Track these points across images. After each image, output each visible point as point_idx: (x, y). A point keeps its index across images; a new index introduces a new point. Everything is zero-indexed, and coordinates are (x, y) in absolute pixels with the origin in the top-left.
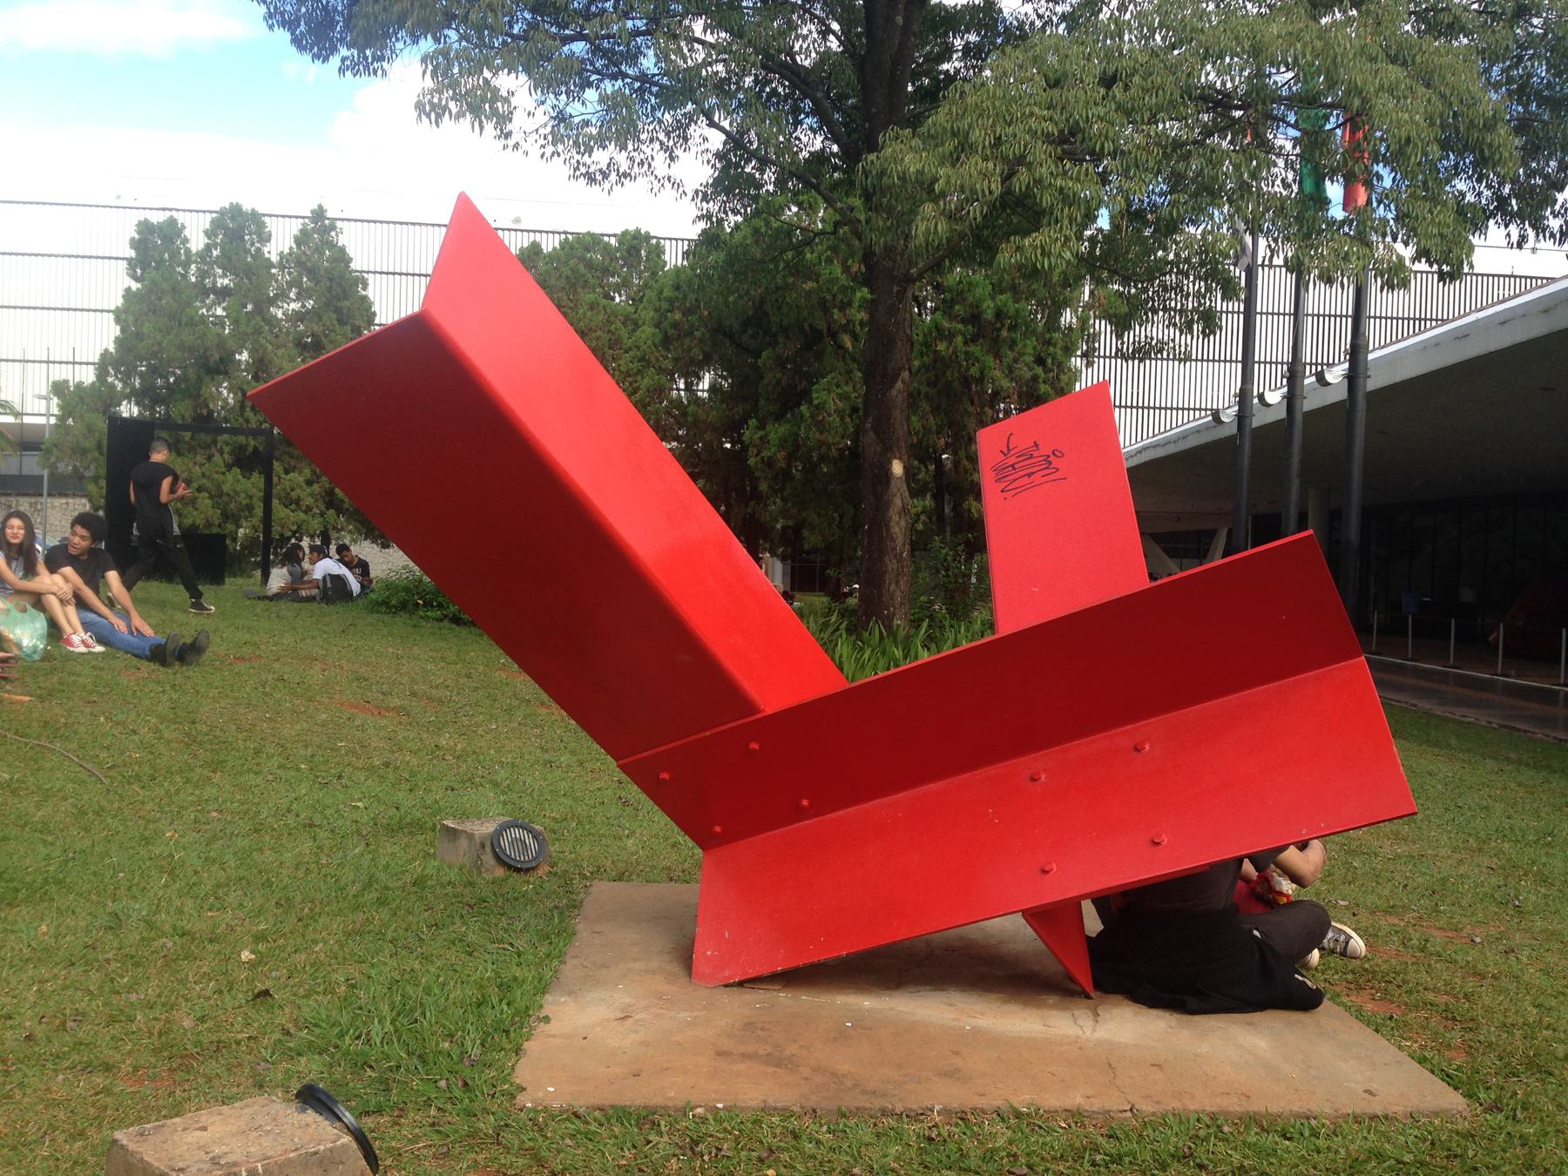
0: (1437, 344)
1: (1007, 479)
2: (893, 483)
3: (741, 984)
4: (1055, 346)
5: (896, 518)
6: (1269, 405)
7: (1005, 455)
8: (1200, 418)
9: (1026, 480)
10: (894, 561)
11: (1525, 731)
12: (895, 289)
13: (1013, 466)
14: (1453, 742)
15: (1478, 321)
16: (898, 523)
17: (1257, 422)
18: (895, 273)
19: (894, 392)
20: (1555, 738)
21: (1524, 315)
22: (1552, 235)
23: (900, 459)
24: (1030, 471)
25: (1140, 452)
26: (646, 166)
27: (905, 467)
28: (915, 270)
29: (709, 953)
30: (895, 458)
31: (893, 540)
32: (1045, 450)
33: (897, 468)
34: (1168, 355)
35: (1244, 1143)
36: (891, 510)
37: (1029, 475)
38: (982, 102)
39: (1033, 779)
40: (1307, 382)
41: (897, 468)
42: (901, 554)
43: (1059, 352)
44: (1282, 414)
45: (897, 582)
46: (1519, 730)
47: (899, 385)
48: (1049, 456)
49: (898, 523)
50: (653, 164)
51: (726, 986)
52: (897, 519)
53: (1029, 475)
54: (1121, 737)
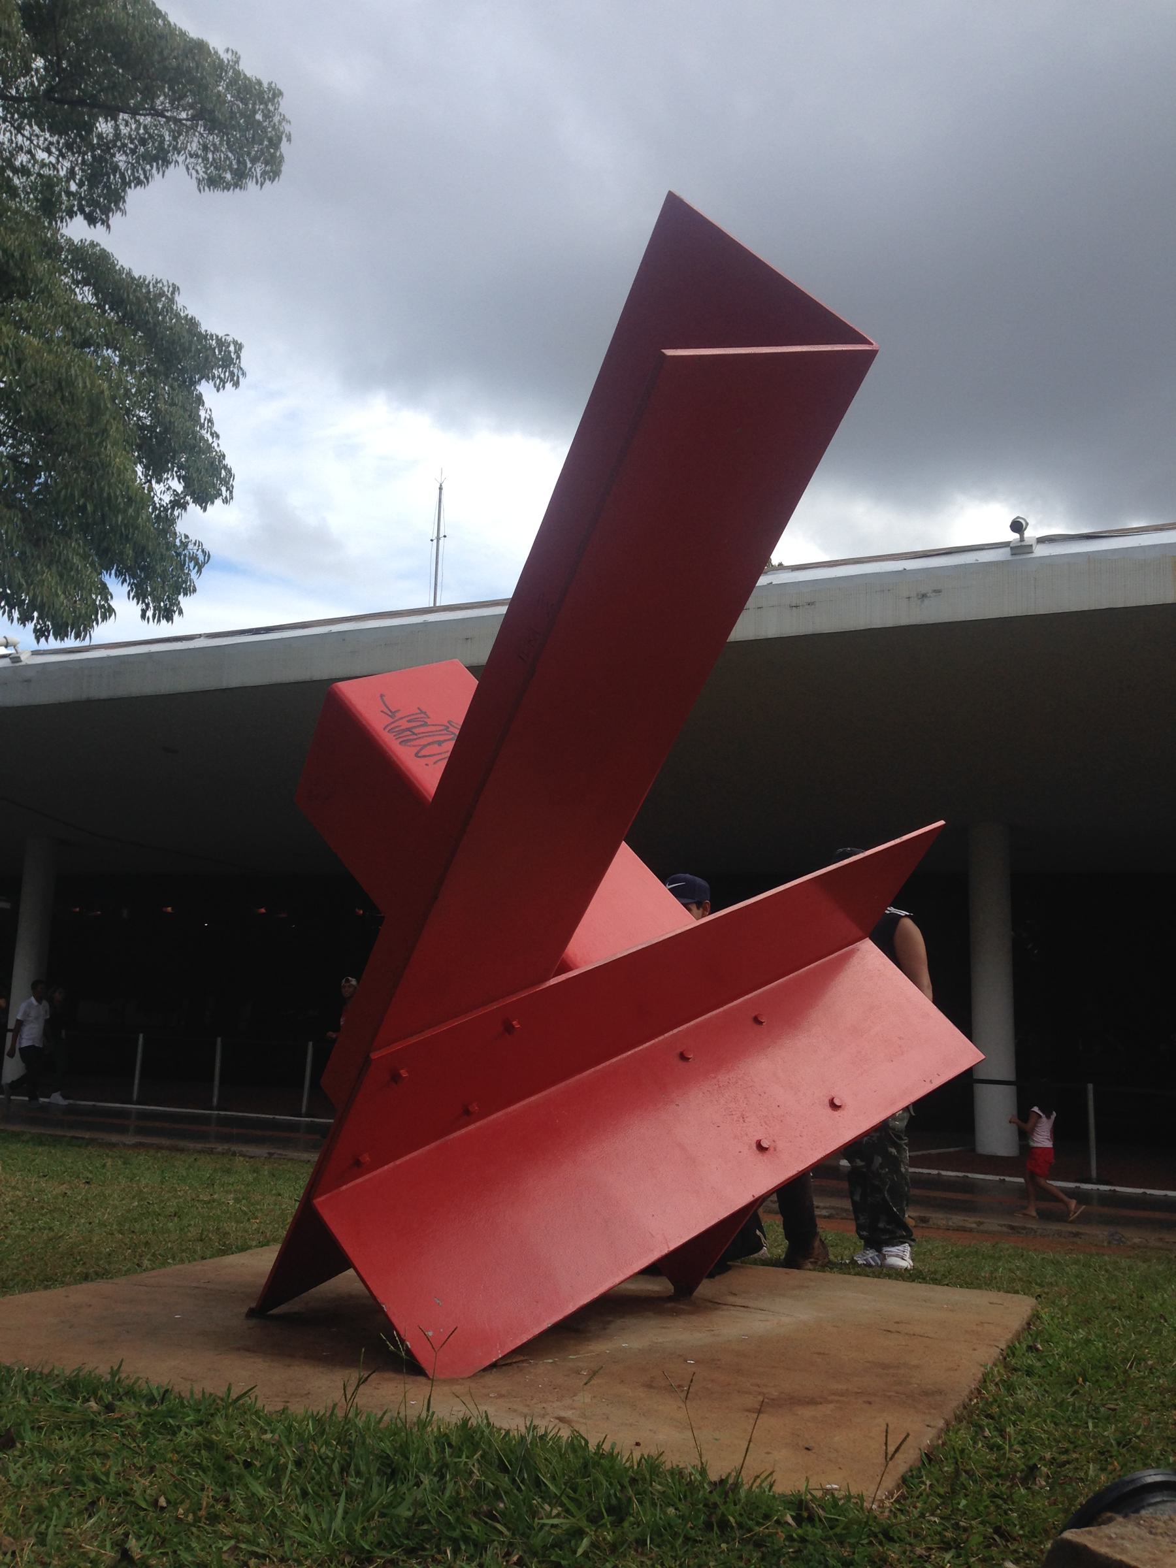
13: (408, 729)
48: (448, 727)
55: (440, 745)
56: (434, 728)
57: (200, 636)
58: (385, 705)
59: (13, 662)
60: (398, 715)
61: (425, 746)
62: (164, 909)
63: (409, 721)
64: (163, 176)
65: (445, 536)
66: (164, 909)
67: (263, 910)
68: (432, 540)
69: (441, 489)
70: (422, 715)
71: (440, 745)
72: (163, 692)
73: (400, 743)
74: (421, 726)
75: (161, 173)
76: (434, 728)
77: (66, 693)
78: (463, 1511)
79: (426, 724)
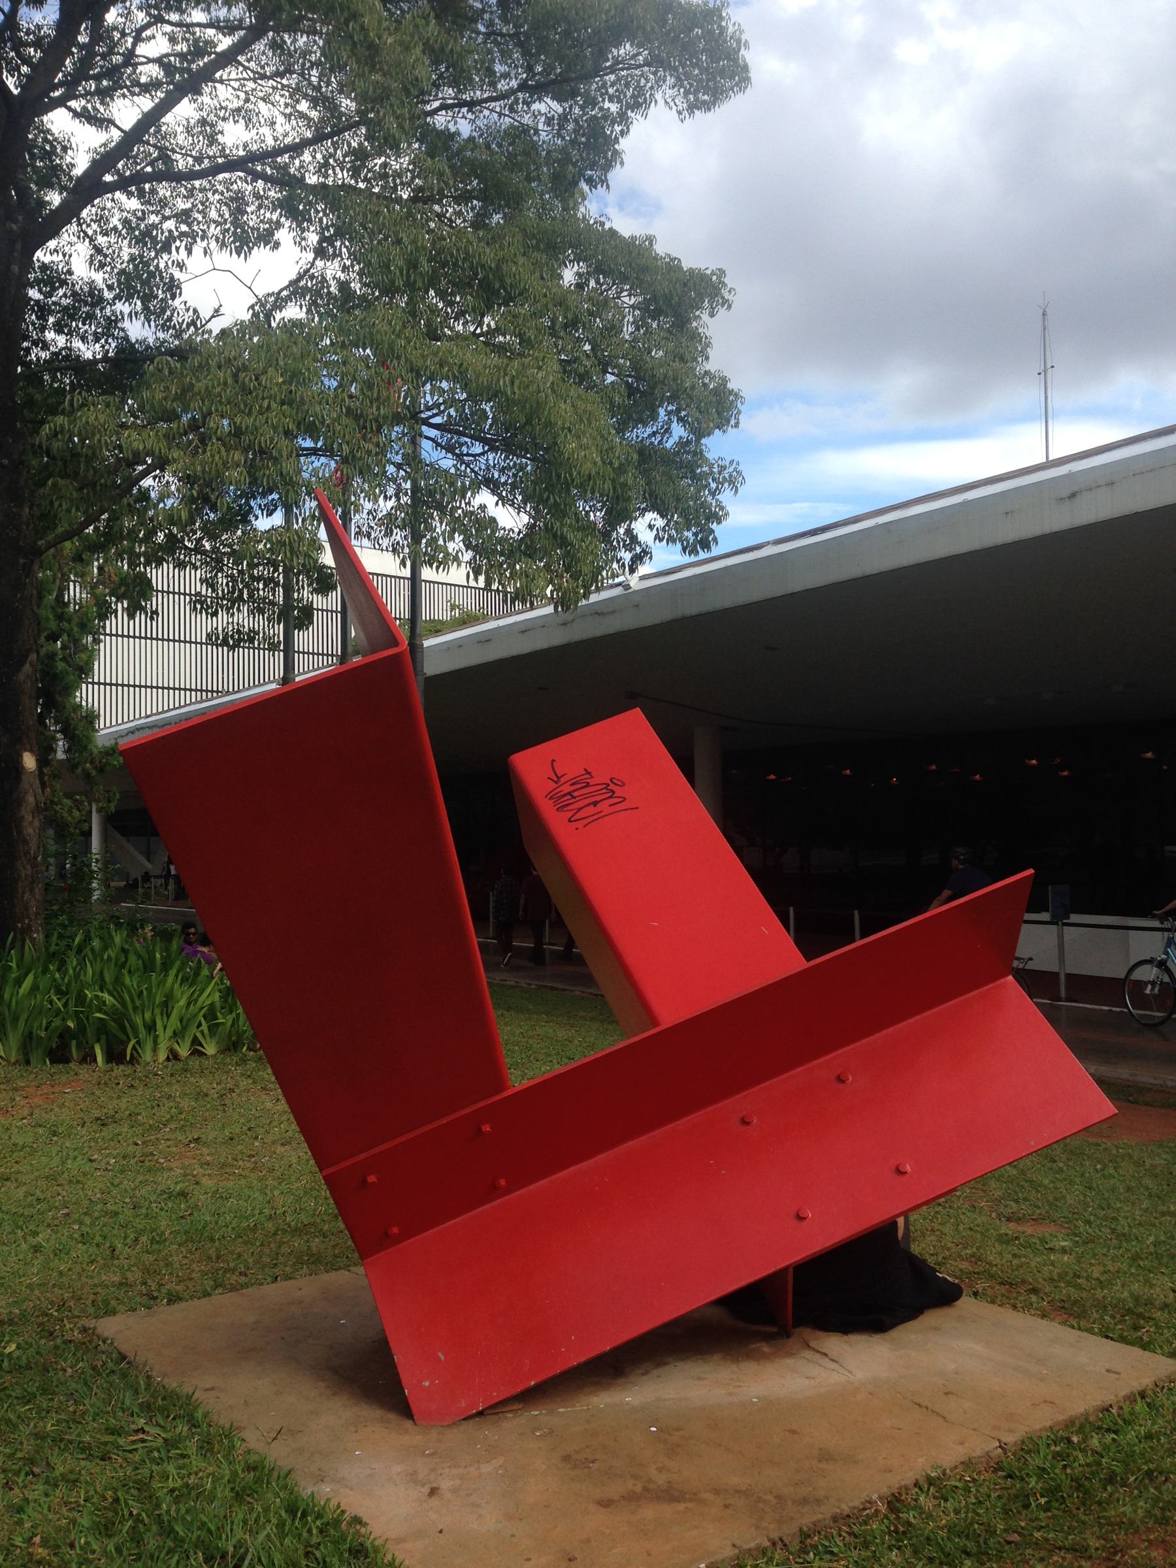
0: (460, 646)
1: (570, 807)
2: (24, 778)
4: (69, 621)
7: (556, 782)
8: (202, 701)
9: (591, 810)
10: (28, 867)
11: (564, 990)
12: (22, 561)
13: (569, 793)
14: (531, 1007)
15: (499, 628)
16: (31, 823)
18: (21, 543)
19: (21, 676)
20: (590, 994)
21: (543, 626)
23: (31, 751)
24: (593, 799)
25: (132, 733)
27: (38, 761)
28: (43, 542)
29: (427, 1384)
30: (26, 750)
31: (26, 842)
32: (600, 777)
34: (259, 645)
36: (23, 809)
37: (595, 804)
38: (213, 387)
39: (745, 1122)
43: (76, 629)
45: (32, 890)
46: (556, 989)
47: (27, 668)
48: (608, 785)
49: (31, 823)
52: (30, 818)
53: (595, 804)
54: (821, 1067)
55: (595, 806)
56: (595, 788)
57: (768, 543)
58: (554, 771)
59: (625, 590)
60: (563, 780)
61: (580, 809)
62: (843, 772)
63: (573, 784)
64: (246, 259)
65: (1052, 367)
66: (843, 772)
67: (934, 767)
68: (1039, 374)
69: (1044, 315)
70: (588, 776)
71: (595, 806)
72: (740, 603)
73: (557, 810)
74: (583, 787)
75: (243, 255)
76: (595, 788)
77: (664, 614)
78: (1158, 1327)
79: (588, 785)
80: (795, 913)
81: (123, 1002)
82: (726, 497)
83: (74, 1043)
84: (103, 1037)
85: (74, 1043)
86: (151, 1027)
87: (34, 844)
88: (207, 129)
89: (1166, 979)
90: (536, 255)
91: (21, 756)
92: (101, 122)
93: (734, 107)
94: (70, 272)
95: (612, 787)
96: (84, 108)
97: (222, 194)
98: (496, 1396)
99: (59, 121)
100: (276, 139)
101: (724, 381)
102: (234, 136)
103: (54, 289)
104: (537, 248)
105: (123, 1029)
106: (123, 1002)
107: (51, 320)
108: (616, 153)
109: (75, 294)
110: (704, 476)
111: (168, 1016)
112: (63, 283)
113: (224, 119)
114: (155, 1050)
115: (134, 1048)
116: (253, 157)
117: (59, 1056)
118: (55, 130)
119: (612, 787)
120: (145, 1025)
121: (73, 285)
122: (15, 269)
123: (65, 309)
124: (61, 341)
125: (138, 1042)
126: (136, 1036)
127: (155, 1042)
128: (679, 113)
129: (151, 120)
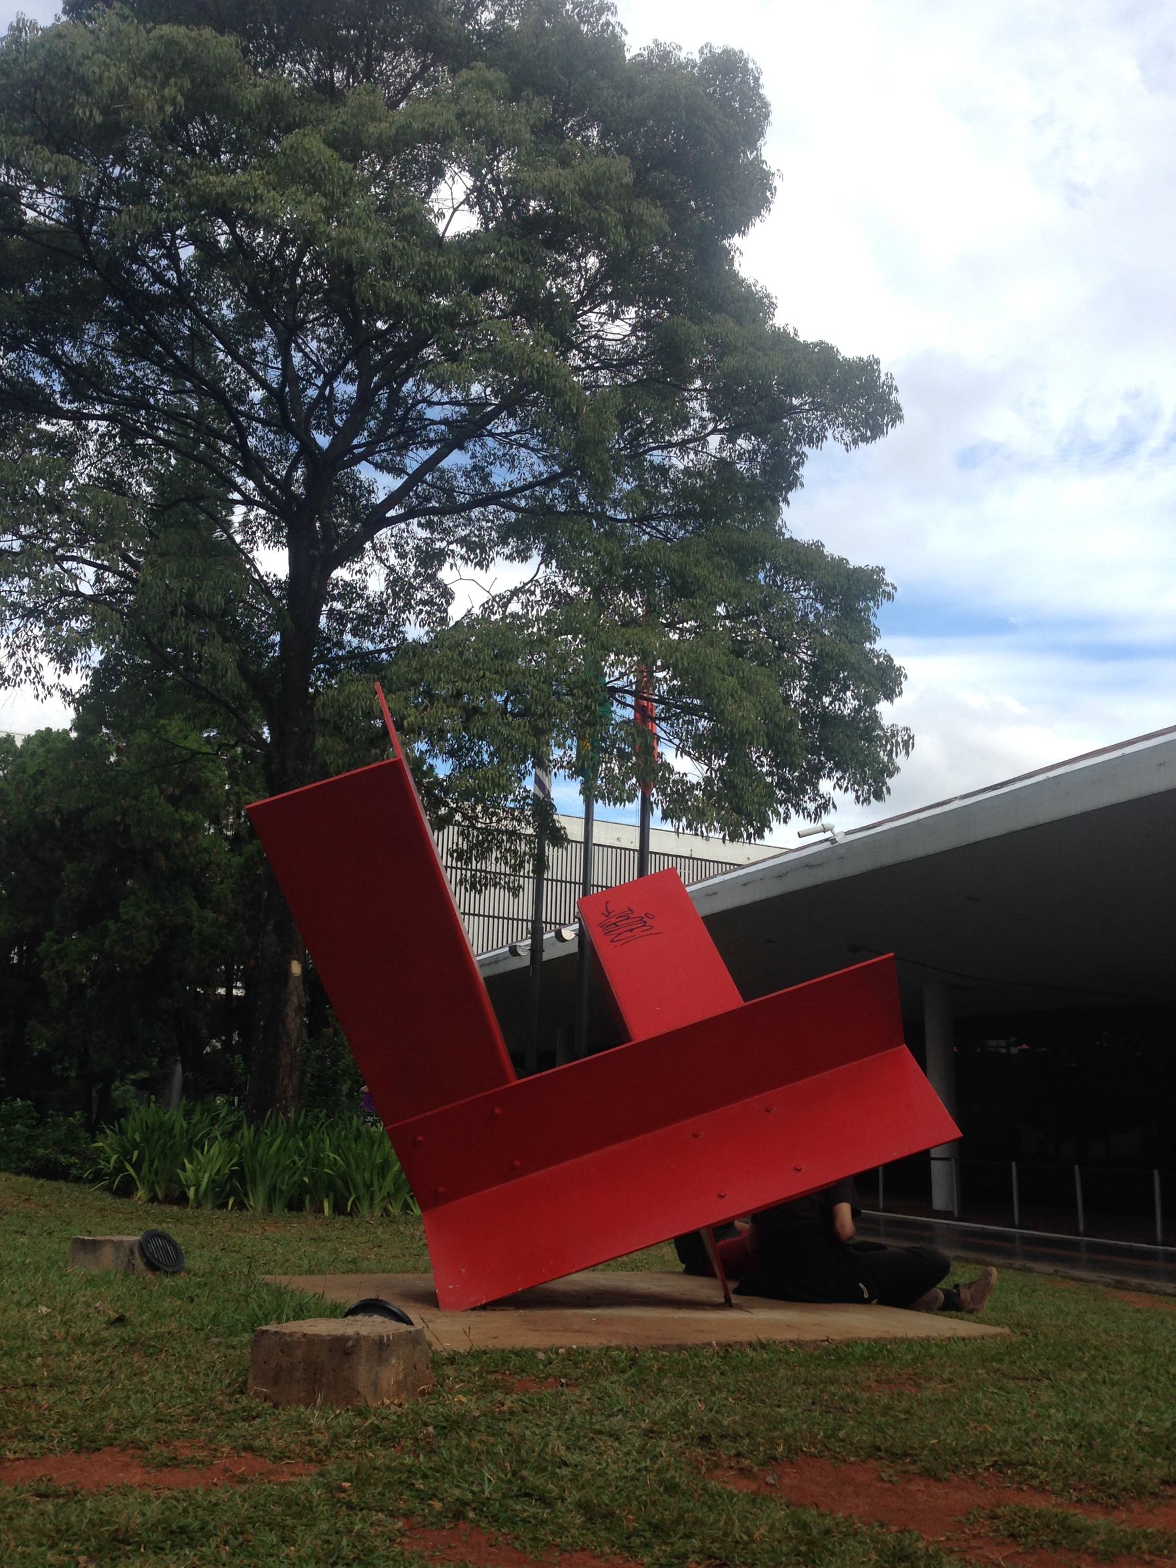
2: (291, 982)
3: (483, 1308)
5: (292, 1014)
6: (564, 940)
9: (629, 934)
17: (547, 956)
22: (809, 815)
26: (33, 674)
33: (296, 968)
35: (704, 1489)
37: (631, 930)
39: (695, 1136)
40: (545, 937)
41: (296, 968)
42: (295, 1049)
44: (574, 948)
50: (42, 673)
51: (473, 1309)
53: (631, 930)
80: (1018, 1169)
81: (348, 1165)
82: (900, 760)
83: (308, 1197)
84: (331, 1195)
85: (308, 1197)
86: (368, 1186)
87: (294, 1036)
88: (479, 471)
89: (541, 795)
90: (717, 559)
91: (290, 964)
92: (397, 471)
93: (894, 434)
94: (365, 587)
95: (645, 919)
96: (383, 460)
97: (493, 522)
98: (495, 1296)
99: (365, 472)
100: (534, 477)
101: (889, 659)
102: (501, 477)
103: (352, 601)
104: (719, 553)
105: (346, 1185)
106: (348, 1165)
107: (349, 625)
108: (797, 478)
109: (368, 605)
110: (879, 738)
111: (384, 1178)
112: (360, 597)
113: (492, 464)
114: (371, 1206)
115: (354, 1202)
116: (514, 492)
117: (295, 1205)
118: (362, 477)
119: (645, 919)
120: (365, 1185)
121: (368, 598)
122: (315, 584)
123: (360, 617)
124: (355, 642)
125: (358, 1198)
126: (356, 1192)
127: (372, 1199)
128: (846, 444)
129: (430, 465)
